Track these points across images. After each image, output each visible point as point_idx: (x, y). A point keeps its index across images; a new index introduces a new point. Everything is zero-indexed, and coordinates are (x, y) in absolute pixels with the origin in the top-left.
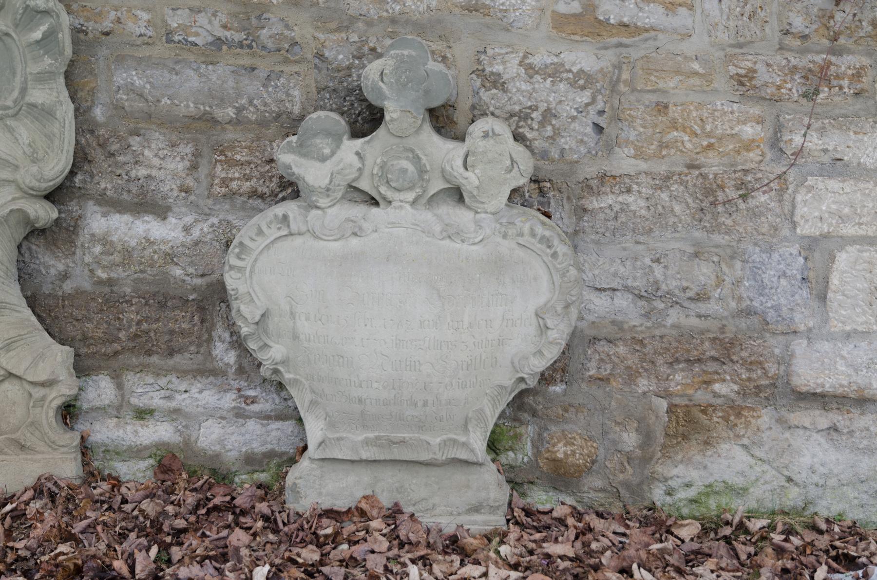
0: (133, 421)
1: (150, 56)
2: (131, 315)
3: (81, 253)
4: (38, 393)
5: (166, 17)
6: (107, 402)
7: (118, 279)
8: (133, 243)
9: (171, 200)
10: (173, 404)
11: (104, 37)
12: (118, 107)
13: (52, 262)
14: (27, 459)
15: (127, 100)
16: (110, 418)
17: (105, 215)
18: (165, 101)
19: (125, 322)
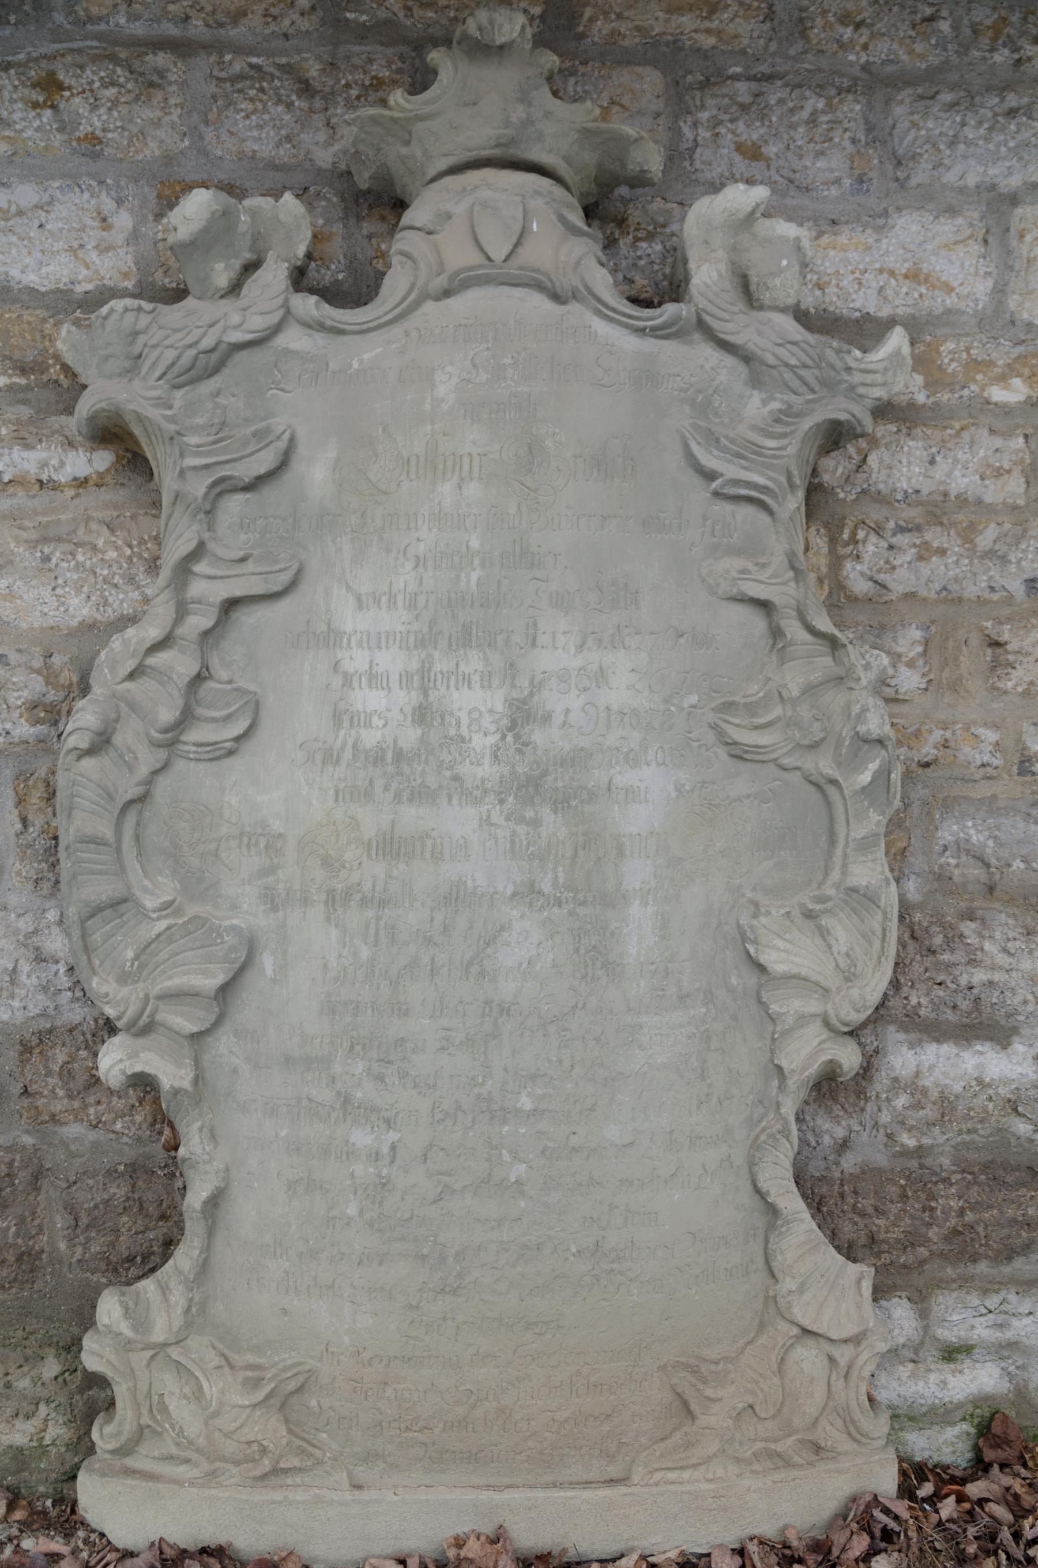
1: (994, 797)
2: (949, 1201)
3: (875, 1108)
4: (843, 1355)
5: (1025, 737)
6: (902, 1340)
7: (932, 1146)
8: (958, 1088)
9: (1021, 1018)
10: (1009, 1335)
11: (920, 771)
12: (942, 877)
13: (827, 1126)
15: (957, 866)
16: (902, 1363)
17: (912, 1046)
18: (1018, 865)
19: (939, 1212)
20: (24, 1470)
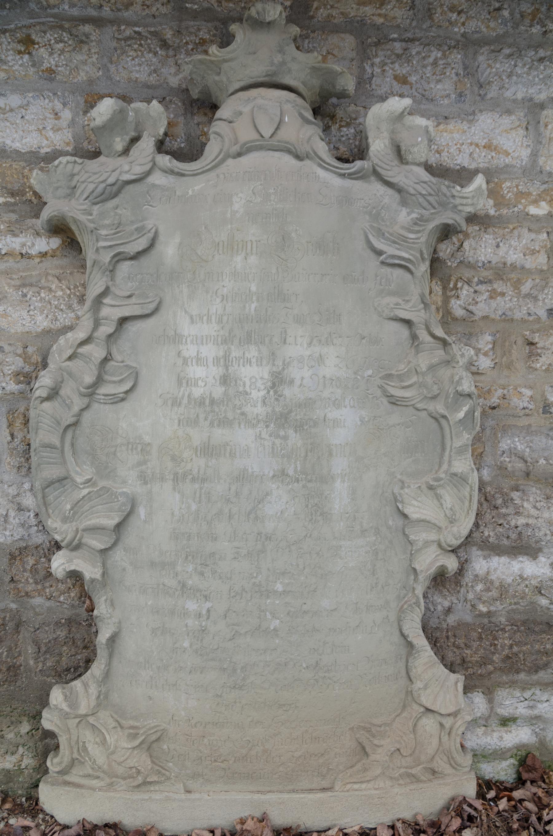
2: (504, 641)
3: (465, 591)
4: (448, 722)
5: (546, 393)
6: (479, 715)
7: (496, 611)
8: (509, 580)
9: (543, 543)
10: (536, 712)
11: (490, 411)
12: (502, 468)
14: (440, 784)
15: (510, 462)
16: (479, 727)
17: (485, 558)
18: (542, 461)
19: (499, 647)
20: (10, 782)
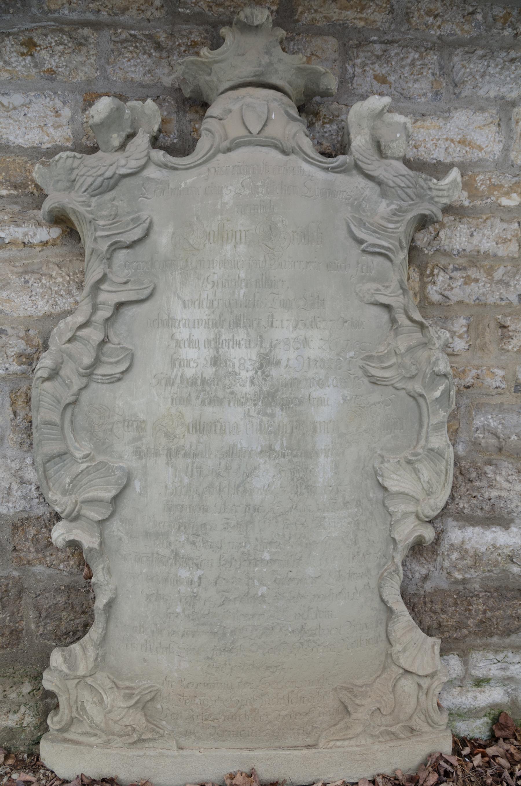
0: (473, 689)
2: (478, 606)
3: (442, 559)
4: (425, 683)
6: (454, 676)
7: (470, 578)
8: (483, 549)
9: (515, 514)
10: (508, 673)
11: (465, 390)
12: (476, 443)
13: (417, 568)
15: (483, 438)
16: (454, 687)
17: (460, 528)
19: (473, 612)
